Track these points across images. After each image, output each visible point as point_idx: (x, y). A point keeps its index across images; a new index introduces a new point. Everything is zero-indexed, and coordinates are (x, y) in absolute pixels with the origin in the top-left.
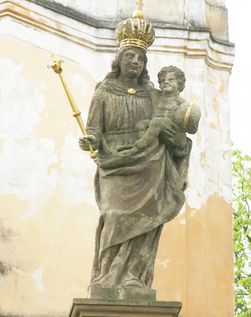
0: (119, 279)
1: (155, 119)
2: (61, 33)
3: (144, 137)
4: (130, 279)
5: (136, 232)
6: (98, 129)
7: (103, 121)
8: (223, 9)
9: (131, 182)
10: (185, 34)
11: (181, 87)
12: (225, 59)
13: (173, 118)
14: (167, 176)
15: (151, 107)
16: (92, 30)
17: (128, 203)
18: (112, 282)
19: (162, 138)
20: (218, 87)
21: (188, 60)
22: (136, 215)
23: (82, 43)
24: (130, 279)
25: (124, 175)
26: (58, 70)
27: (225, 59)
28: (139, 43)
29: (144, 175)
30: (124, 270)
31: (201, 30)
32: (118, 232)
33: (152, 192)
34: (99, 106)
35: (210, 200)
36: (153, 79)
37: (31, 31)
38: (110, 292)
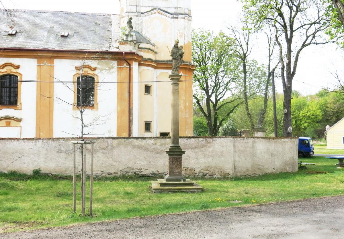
0: (175, 72)
1: (179, 53)
2: (165, 16)
3: (178, 55)
4: (176, 72)
5: (177, 66)
6: (172, 54)
7: (173, 53)
8: (191, 11)
9: (176, 60)
10: (184, 15)
11: (182, 48)
12: (191, 19)
13: (181, 52)
14: (180, 59)
15: (179, 51)
16: (170, 15)
17: (176, 63)
18: (174, 72)
19: (180, 55)
20: (190, 24)
21: (185, 20)
22: (177, 64)
23: (169, 17)
24: (176, 72)
25: (175, 60)
26: (168, 47)
27: (191, 19)
28: (177, 43)
29: (178, 60)
30: (175, 71)
31: (187, 15)
32: (175, 66)
33: (179, 62)
34: (173, 51)
35: (188, 42)
36: (179, 47)
37: (161, 15)
38: (174, 74)
